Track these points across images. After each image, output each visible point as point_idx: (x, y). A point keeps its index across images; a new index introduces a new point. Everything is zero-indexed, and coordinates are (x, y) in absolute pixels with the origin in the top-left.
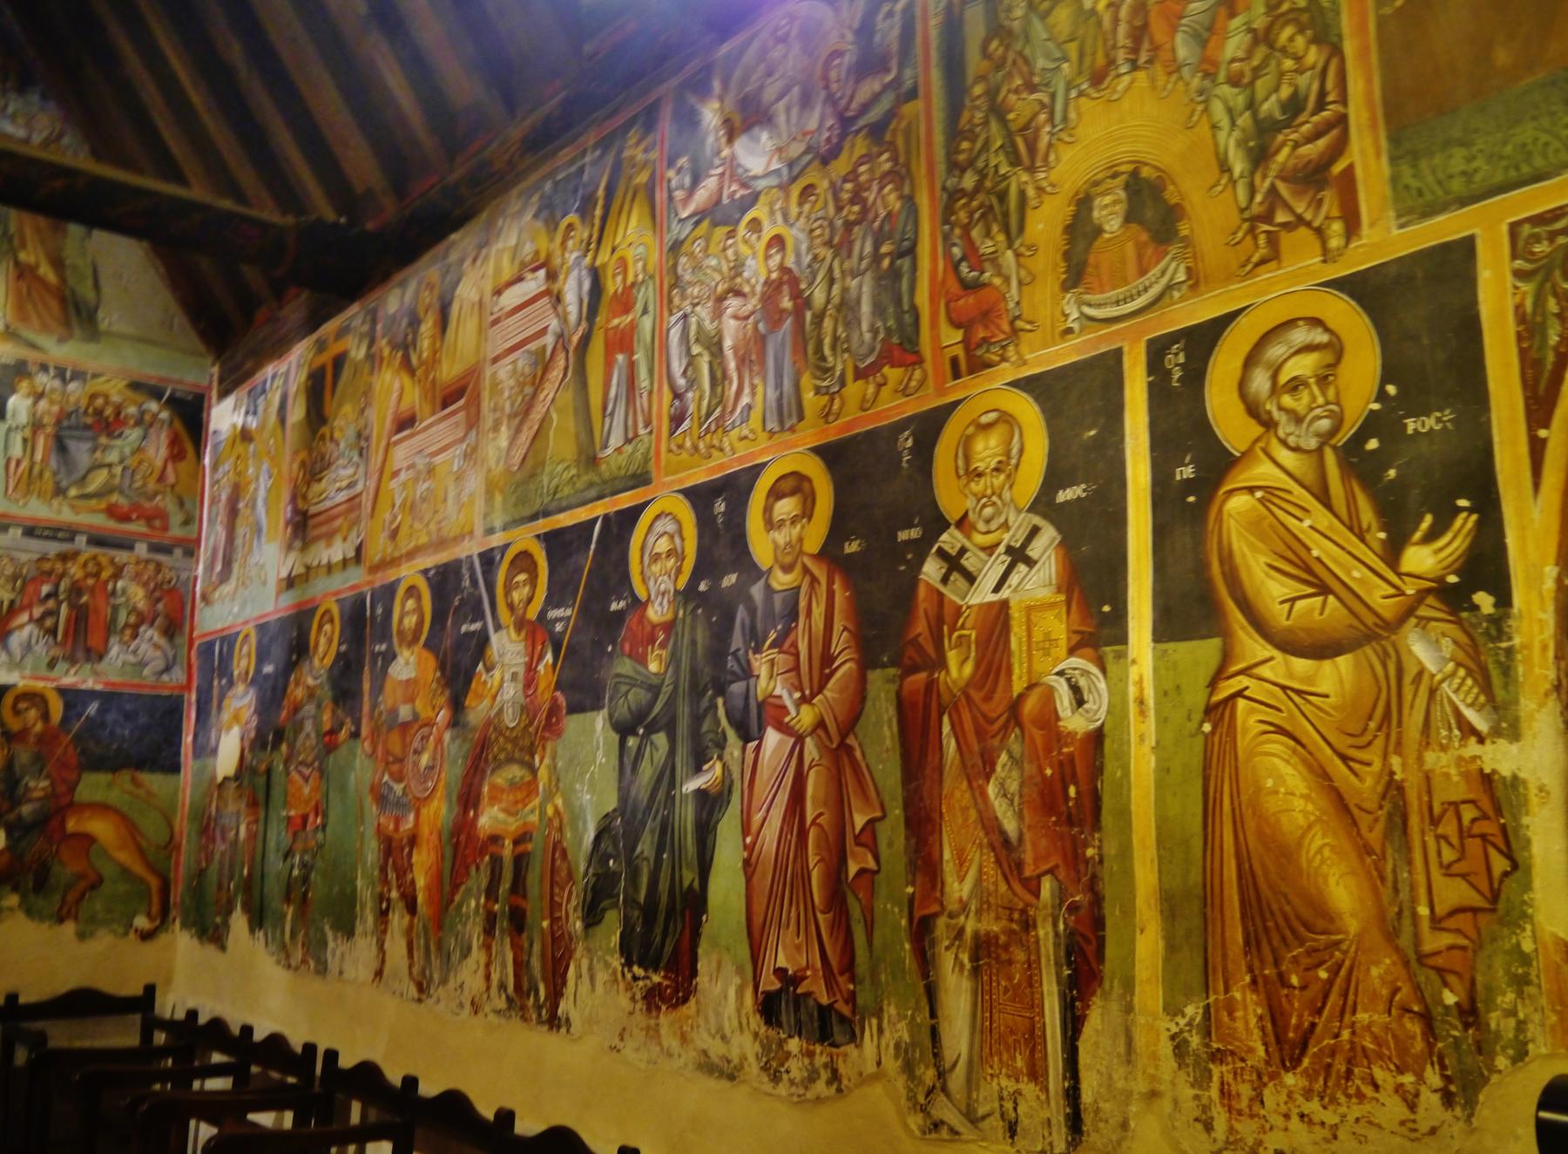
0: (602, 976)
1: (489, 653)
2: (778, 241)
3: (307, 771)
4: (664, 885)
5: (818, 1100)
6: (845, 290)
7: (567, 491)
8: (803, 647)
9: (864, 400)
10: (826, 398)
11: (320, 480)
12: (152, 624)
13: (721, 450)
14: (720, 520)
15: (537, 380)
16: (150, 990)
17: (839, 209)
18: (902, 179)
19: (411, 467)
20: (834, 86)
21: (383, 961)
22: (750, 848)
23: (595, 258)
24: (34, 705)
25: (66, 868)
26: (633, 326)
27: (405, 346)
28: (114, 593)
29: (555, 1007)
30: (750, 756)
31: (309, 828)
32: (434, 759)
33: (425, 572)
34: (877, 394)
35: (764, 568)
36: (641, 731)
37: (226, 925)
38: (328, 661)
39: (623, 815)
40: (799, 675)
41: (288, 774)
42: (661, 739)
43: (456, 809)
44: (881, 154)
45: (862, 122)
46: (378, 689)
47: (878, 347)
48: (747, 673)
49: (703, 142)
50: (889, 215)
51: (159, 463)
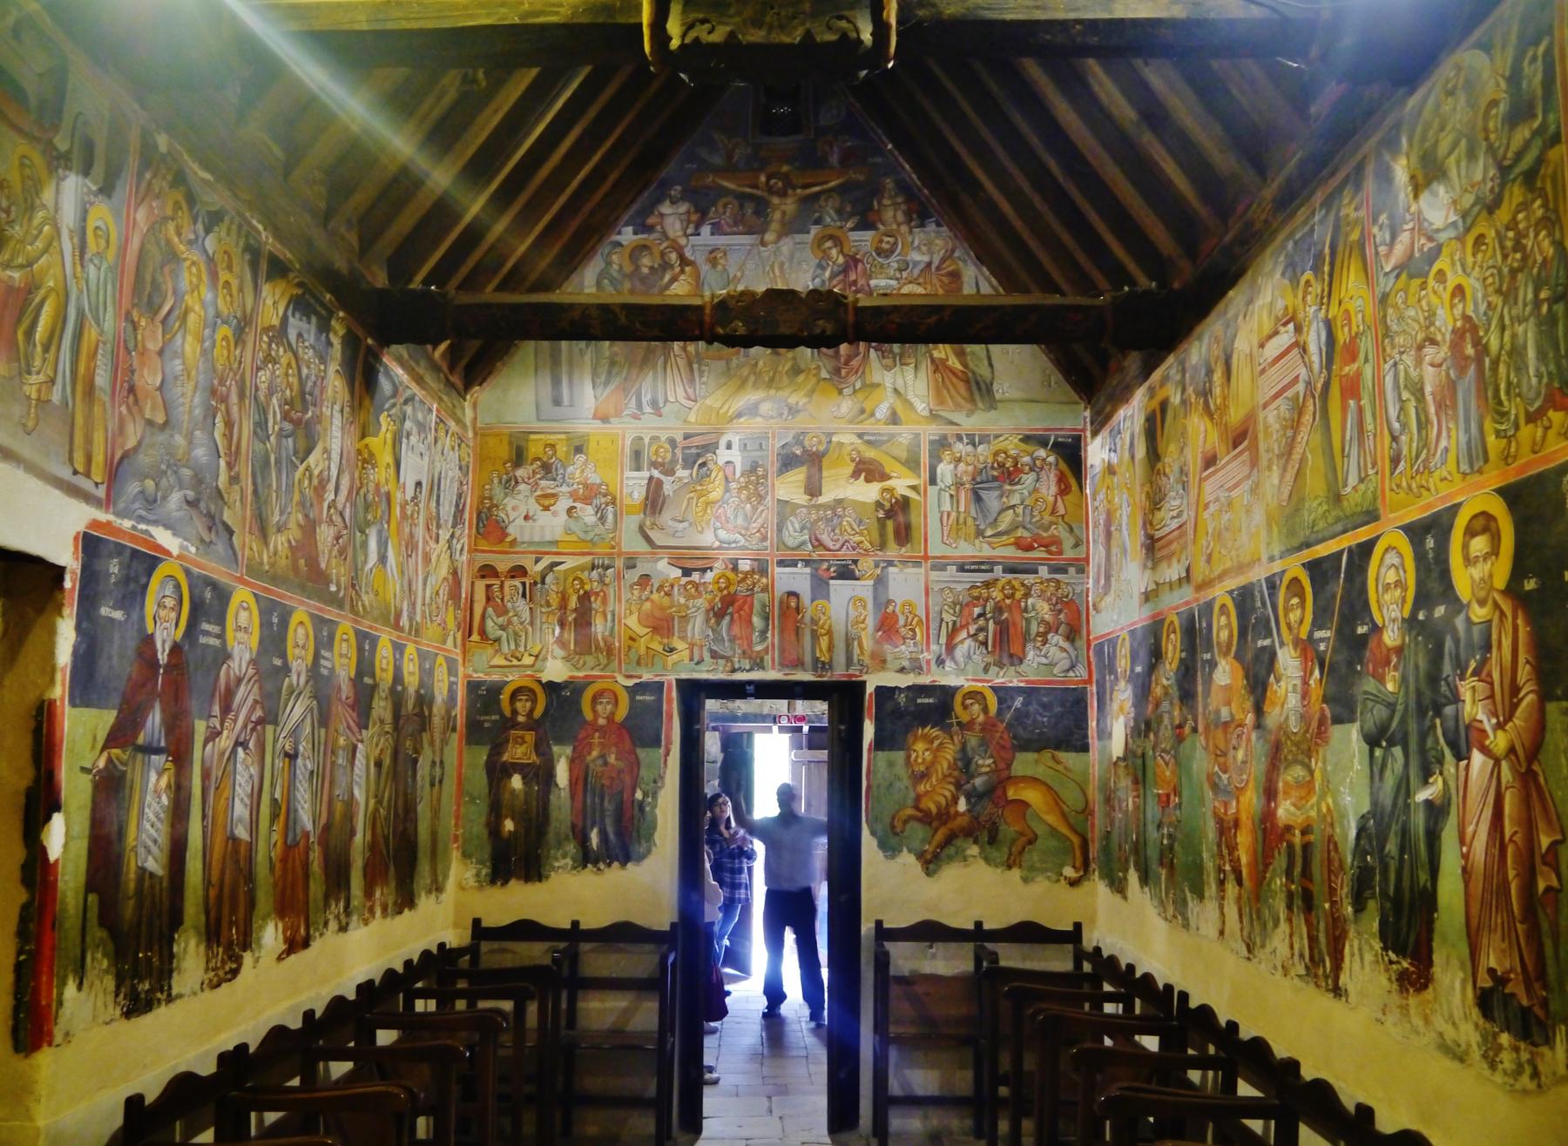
0: (1368, 957)
1: (1277, 666)
2: (1459, 290)
3: (1167, 758)
4: (1406, 884)
5: (1525, 1092)
6: (1514, 336)
7: (1321, 525)
8: (1496, 676)
9: (1534, 443)
10: (1505, 441)
11: (1159, 509)
12: (1056, 632)
13: (1428, 490)
14: (1431, 555)
15: (1295, 425)
16: (1078, 926)
17: (1505, 257)
18: (1553, 224)
19: (1217, 500)
20: (1492, 136)
21: (1224, 922)
22: (1465, 857)
23: (1327, 311)
24: (978, 702)
25: (1009, 829)
26: (1359, 374)
27: (1205, 393)
28: (1026, 610)
29: (1336, 979)
30: (1462, 773)
31: (1171, 805)
32: (1246, 755)
33: (1231, 592)
34: (1544, 437)
35: (1465, 602)
36: (1384, 744)
37: (1125, 878)
38: (1175, 665)
39: (1374, 817)
40: (1494, 703)
41: (1155, 758)
42: (1397, 751)
43: (1263, 801)
44: (1533, 201)
45: (1517, 170)
46: (1207, 693)
47: (1543, 391)
48: (1456, 699)
49: (1396, 197)
50: (1545, 260)
51: (1051, 499)
